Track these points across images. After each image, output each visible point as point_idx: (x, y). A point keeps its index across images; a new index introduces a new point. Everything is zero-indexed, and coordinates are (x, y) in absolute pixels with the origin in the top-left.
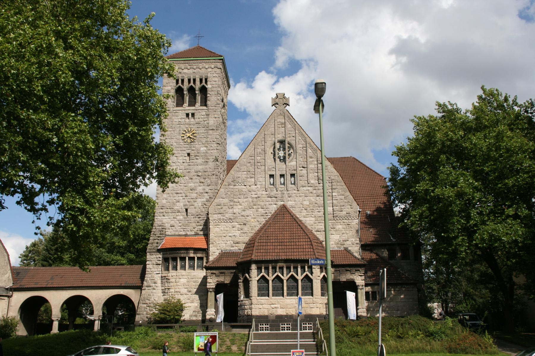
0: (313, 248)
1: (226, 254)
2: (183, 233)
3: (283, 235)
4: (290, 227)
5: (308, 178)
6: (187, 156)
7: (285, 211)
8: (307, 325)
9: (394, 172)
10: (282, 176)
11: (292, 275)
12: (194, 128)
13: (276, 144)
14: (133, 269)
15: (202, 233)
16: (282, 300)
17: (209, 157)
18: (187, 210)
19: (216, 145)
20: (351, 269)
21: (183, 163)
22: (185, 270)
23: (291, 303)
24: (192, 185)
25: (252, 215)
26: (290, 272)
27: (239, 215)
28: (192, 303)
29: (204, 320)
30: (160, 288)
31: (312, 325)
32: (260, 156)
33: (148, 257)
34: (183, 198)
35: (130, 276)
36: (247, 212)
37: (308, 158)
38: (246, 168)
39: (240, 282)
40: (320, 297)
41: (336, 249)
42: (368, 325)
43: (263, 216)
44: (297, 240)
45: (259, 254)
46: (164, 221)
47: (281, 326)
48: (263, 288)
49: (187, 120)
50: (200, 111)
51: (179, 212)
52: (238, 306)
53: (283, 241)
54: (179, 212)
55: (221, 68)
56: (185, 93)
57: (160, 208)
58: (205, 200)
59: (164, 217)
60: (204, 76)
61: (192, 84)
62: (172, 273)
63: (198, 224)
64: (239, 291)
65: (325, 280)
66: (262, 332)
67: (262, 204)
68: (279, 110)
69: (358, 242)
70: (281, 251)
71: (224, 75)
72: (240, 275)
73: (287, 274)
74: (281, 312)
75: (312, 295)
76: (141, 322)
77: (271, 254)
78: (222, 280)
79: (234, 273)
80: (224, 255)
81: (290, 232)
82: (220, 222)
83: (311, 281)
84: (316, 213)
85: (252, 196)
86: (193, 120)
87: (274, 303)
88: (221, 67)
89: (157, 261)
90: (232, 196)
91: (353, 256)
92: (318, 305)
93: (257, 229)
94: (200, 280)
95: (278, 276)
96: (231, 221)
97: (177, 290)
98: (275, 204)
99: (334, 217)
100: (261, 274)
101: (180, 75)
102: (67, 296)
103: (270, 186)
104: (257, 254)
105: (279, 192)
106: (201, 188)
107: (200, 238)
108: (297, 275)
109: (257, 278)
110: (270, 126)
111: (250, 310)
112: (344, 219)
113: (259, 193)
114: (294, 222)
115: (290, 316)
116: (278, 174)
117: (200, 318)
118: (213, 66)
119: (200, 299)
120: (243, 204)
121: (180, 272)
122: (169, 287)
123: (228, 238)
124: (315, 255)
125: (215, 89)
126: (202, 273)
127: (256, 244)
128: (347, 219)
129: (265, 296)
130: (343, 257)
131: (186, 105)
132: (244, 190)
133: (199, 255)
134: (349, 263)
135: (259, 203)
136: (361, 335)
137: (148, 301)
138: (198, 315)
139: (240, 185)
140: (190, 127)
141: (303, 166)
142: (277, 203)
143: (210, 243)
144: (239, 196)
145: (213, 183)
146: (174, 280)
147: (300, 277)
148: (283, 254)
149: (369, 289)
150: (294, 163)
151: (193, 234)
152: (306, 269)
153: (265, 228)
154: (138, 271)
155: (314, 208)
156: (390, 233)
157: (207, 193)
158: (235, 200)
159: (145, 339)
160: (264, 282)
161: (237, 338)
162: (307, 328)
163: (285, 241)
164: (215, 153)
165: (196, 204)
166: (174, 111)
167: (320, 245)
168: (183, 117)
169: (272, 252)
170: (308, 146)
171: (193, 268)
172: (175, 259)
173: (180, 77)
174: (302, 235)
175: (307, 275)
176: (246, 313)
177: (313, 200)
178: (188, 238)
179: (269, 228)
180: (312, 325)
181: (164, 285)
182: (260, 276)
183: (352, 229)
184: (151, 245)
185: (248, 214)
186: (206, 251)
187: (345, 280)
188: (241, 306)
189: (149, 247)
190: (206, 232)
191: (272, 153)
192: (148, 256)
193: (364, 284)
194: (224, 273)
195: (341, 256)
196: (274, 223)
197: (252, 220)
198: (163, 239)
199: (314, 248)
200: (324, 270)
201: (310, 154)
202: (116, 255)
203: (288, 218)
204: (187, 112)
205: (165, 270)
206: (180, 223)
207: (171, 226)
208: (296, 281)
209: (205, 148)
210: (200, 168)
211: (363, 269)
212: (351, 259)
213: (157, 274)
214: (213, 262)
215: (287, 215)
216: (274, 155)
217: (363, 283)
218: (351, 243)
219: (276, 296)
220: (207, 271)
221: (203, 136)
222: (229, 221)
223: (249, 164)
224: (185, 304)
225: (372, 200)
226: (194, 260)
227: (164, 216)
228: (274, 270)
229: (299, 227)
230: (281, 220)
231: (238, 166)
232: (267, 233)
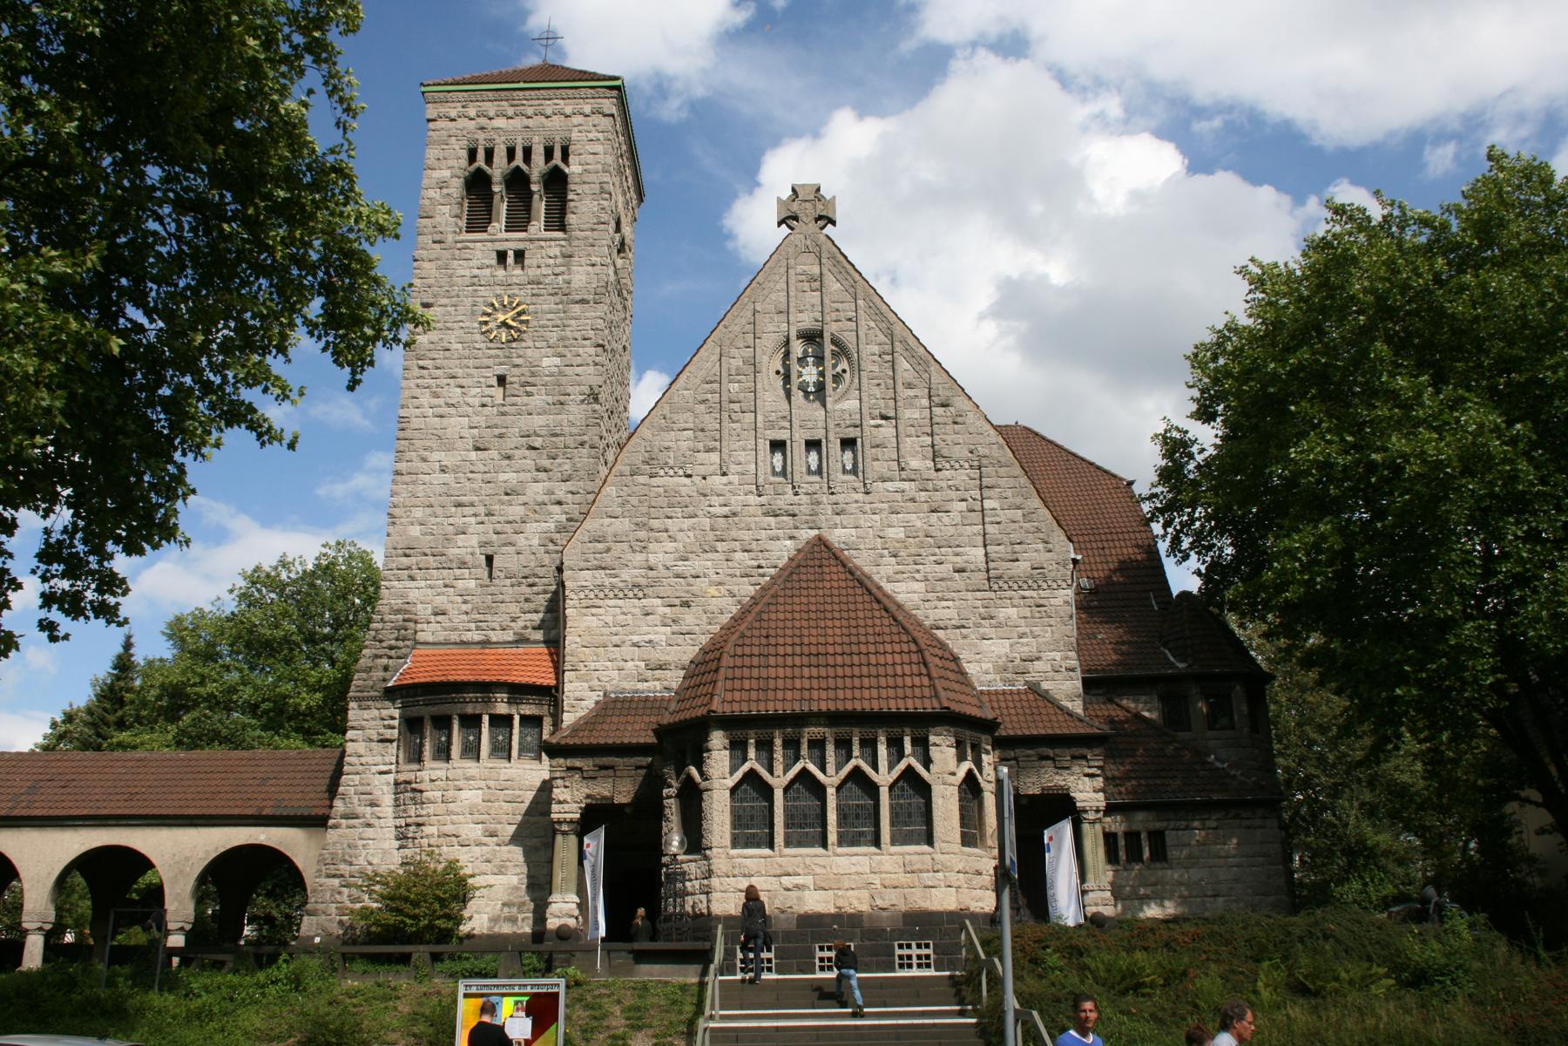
0: (929, 676)
1: (619, 705)
2: (477, 636)
3: (820, 631)
4: (844, 607)
5: (902, 452)
6: (495, 383)
7: (825, 555)
8: (914, 951)
9: (1175, 447)
10: (813, 445)
11: (857, 769)
12: (522, 295)
13: (792, 343)
14: (307, 762)
15: (539, 636)
16: (818, 860)
17: (570, 389)
18: (489, 560)
19: (592, 351)
20: (1058, 751)
21: (484, 405)
22: (478, 759)
23: (854, 869)
24: (509, 477)
25: (711, 572)
26: (849, 757)
27: (665, 573)
28: (501, 873)
29: (539, 935)
30: (391, 822)
31: (930, 951)
32: (739, 382)
33: (351, 714)
34: (479, 519)
35: (296, 782)
36: (696, 564)
37: (900, 387)
38: (691, 420)
39: (669, 797)
40: (956, 846)
41: (1000, 687)
42: (1167, 945)
43: (747, 576)
44: (872, 648)
45: (737, 695)
46: (413, 595)
47: (898, 952)
48: (752, 816)
49: (501, 272)
50: (543, 243)
51: (463, 565)
52: (661, 884)
53: (822, 649)
54: (463, 565)
55: (613, 116)
56: (496, 188)
57: (400, 552)
58: (552, 526)
59: (412, 584)
60: (558, 138)
61: (519, 160)
62: (432, 771)
63: (527, 606)
64: (665, 830)
65: (970, 787)
67: (746, 536)
68: (802, 237)
69: (1074, 663)
70: (815, 683)
71: (624, 147)
72: (669, 772)
73: (839, 767)
74: (817, 902)
75: (929, 840)
76: (317, 940)
77: (780, 695)
78: (607, 793)
79: (649, 767)
80: (611, 706)
81: (845, 623)
82: (601, 595)
83: (924, 789)
84: (928, 568)
85: (711, 509)
86: (518, 271)
87: (791, 870)
88: (614, 110)
89: (382, 731)
90: (644, 510)
91: (1061, 708)
92: (953, 878)
93: (725, 619)
94: (530, 796)
95: (804, 771)
96: (640, 594)
97: (449, 829)
98: (791, 538)
99: (989, 579)
100: (746, 767)
101: (481, 136)
102: (76, 846)
103: (772, 479)
104: (729, 696)
105: (802, 496)
106: (539, 487)
107: (534, 651)
108: (875, 768)
109: (731, 782)
110: (771, 284)
111: (703, 897)
112: (1025, 586)
113: (736, 501)
114: (859, 591)
115: (851, 916)
116: (800, 437)
117: (527, 929)
118: (587, 109)
119: (528, 861)
120: (680, 536)
121: (460, 766)
122: (420, 820)
123: (627, 650)
124: (937, 696)
125: (592, 178)
126: (535, 772)
127: (727, 661)
128: (1035, 586)
129: (758, 846)
130: (1027, 711)
131: (498, 227)
132: (684, 491)
133: (528, 710)
134: (1050, 732)
135: (734, 533)
136: (1152, 985)
137: (348, 868)
138: (520, 916)
140: (510, 292)
141: (883, 412)
142: (795, 533)
143: (567, 666)
144: (668, 511)
145: (582, 473)
146: (439, 794)
147: (884, 777)
148: (824, 694)
149: (1116, 824)
150: (852, 404)
151: (510, 639)
152: (908, 748)
153: (757, 609)
154: (325, 768)
155: (922, 551)
156: (1165, 645)
157: (559, 503)
158: (655, 524)
159: (285, 1003)
160: (755, 795)
161: (655, 1000)
162: (915, 961)
163: (831, 650)
164: (590, 375)
165: (521, 540)
166: (459, 245)
167: (952, 666)
168: (487, 262)
169: (785, 689)
170: (897, 349)
171: (506, 754)
172: (443, 723)
173: (482, 142)
174: (887, 630)
175: (909, 768)
176: (688, 908)
177: (919, 524)
178: (493, 651)
179: (773, 608)
180: (930, 951)
181: (405, 811)
182: (739, 774)
183: (1052, 621)
184: (364, 675)
185: (700, 571)
186: (551, 695)
187: (1037, 791)
188: (672, 878)
189: (358, 680)
190: (553, 632)
191: (778, 372)
192: (354, 714)
193: (1102, 805)
194: (612, 767)
195: (1020, 711)
196: (789, 592)
197: (713, 591)
198: (405, 657)
199: (934, 674)
200: (969, 751)
201: (905, 374)
202: (287, 737)
203: (835, 577)
204: (501, 246)
205: (410, 761)
206: (465, 602)
207: (436, 614)
208: (872, 789)
209: (557, 361)
210: (538, 421)
211: (1097, 751)
212: (1054, 718)
213: (381, 773)
214: (576, 729)
215: (834, 569)
216: (787, 379)
217: (1099, 800)
218: (1049, 669)
219: (800, 844)
220: (554, 762)
221: (550, 323)
222: (631, 594)
223: (702, 407)
224: (472, 876)
225: (1094, 545)
226: (511, 726)
227: (412, 578)
228: (790, 752)
229: (876, 606)
230: (812, 585)
231: (666, 412)
232: (765, 624)
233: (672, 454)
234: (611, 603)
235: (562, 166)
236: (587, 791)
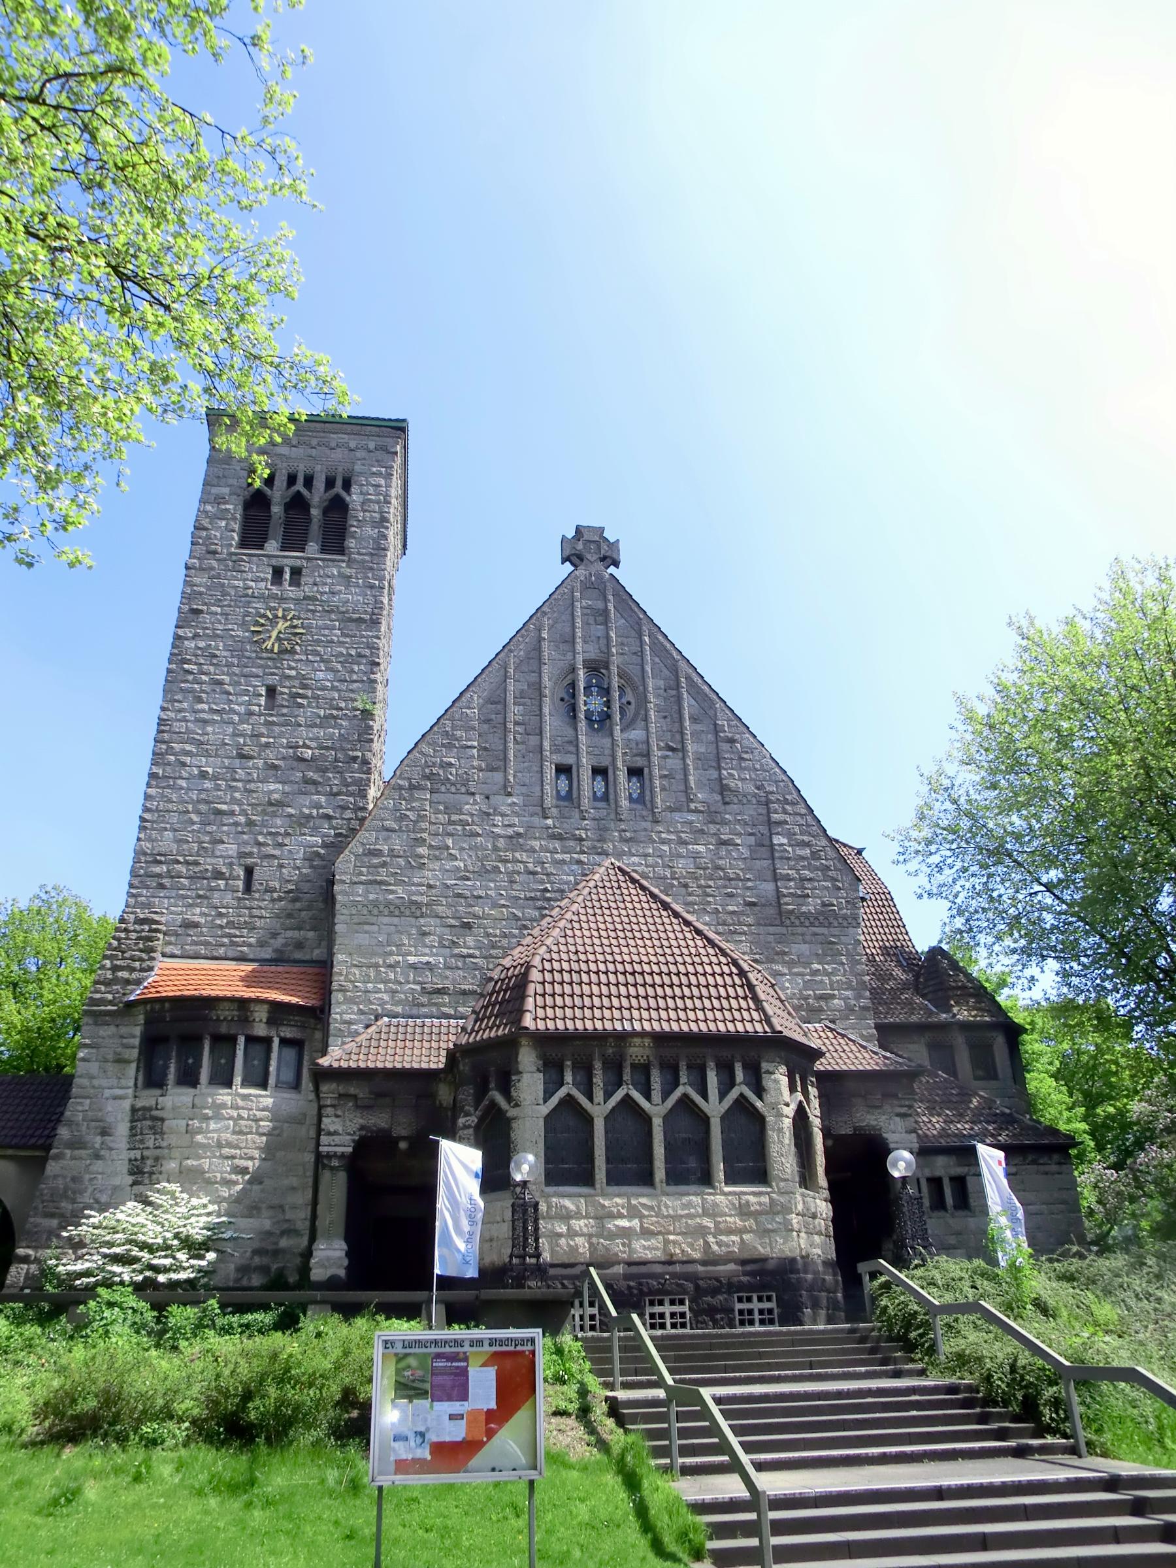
8: (756, 1305)
11: (685, 1097)
18: (249, 872)
30: (125, 1155)
36: (476, 886)
49: (275, 590)
51: (218, 875)
54: (218, 875)
60: (340, 469)
61: (299, 486)
62: (176, 1098)
66: (751, 1329)
73: (666, 1095)
82: (375, 912)
100: (562, 1093)
108: (705, 1096)
109: (545, 1110)
118: (372, 446)
127: (535, 975)
131: (272, 547)
133: (288, 1033)
139: (453, 789)
151: (268, 956)
152: (739, 1075)
162: (757, 1317)
180: (772, 1305)
181: (142, 1141)
182: (554, 1101)
187: (850, 1131)
216: (573, 708)
222: (407, 912)
233: (454, 771)
234: (386, 920)
235: (344, 494)
236: (361, 1121)
